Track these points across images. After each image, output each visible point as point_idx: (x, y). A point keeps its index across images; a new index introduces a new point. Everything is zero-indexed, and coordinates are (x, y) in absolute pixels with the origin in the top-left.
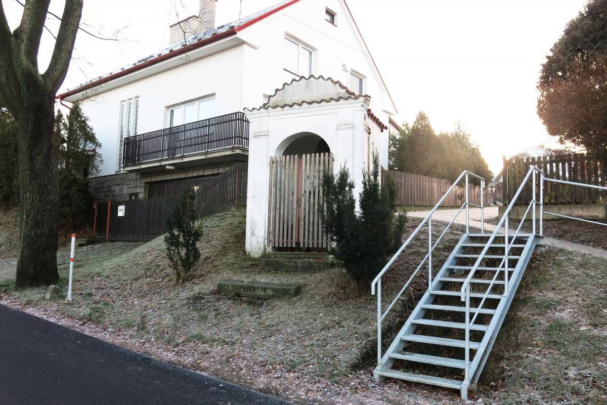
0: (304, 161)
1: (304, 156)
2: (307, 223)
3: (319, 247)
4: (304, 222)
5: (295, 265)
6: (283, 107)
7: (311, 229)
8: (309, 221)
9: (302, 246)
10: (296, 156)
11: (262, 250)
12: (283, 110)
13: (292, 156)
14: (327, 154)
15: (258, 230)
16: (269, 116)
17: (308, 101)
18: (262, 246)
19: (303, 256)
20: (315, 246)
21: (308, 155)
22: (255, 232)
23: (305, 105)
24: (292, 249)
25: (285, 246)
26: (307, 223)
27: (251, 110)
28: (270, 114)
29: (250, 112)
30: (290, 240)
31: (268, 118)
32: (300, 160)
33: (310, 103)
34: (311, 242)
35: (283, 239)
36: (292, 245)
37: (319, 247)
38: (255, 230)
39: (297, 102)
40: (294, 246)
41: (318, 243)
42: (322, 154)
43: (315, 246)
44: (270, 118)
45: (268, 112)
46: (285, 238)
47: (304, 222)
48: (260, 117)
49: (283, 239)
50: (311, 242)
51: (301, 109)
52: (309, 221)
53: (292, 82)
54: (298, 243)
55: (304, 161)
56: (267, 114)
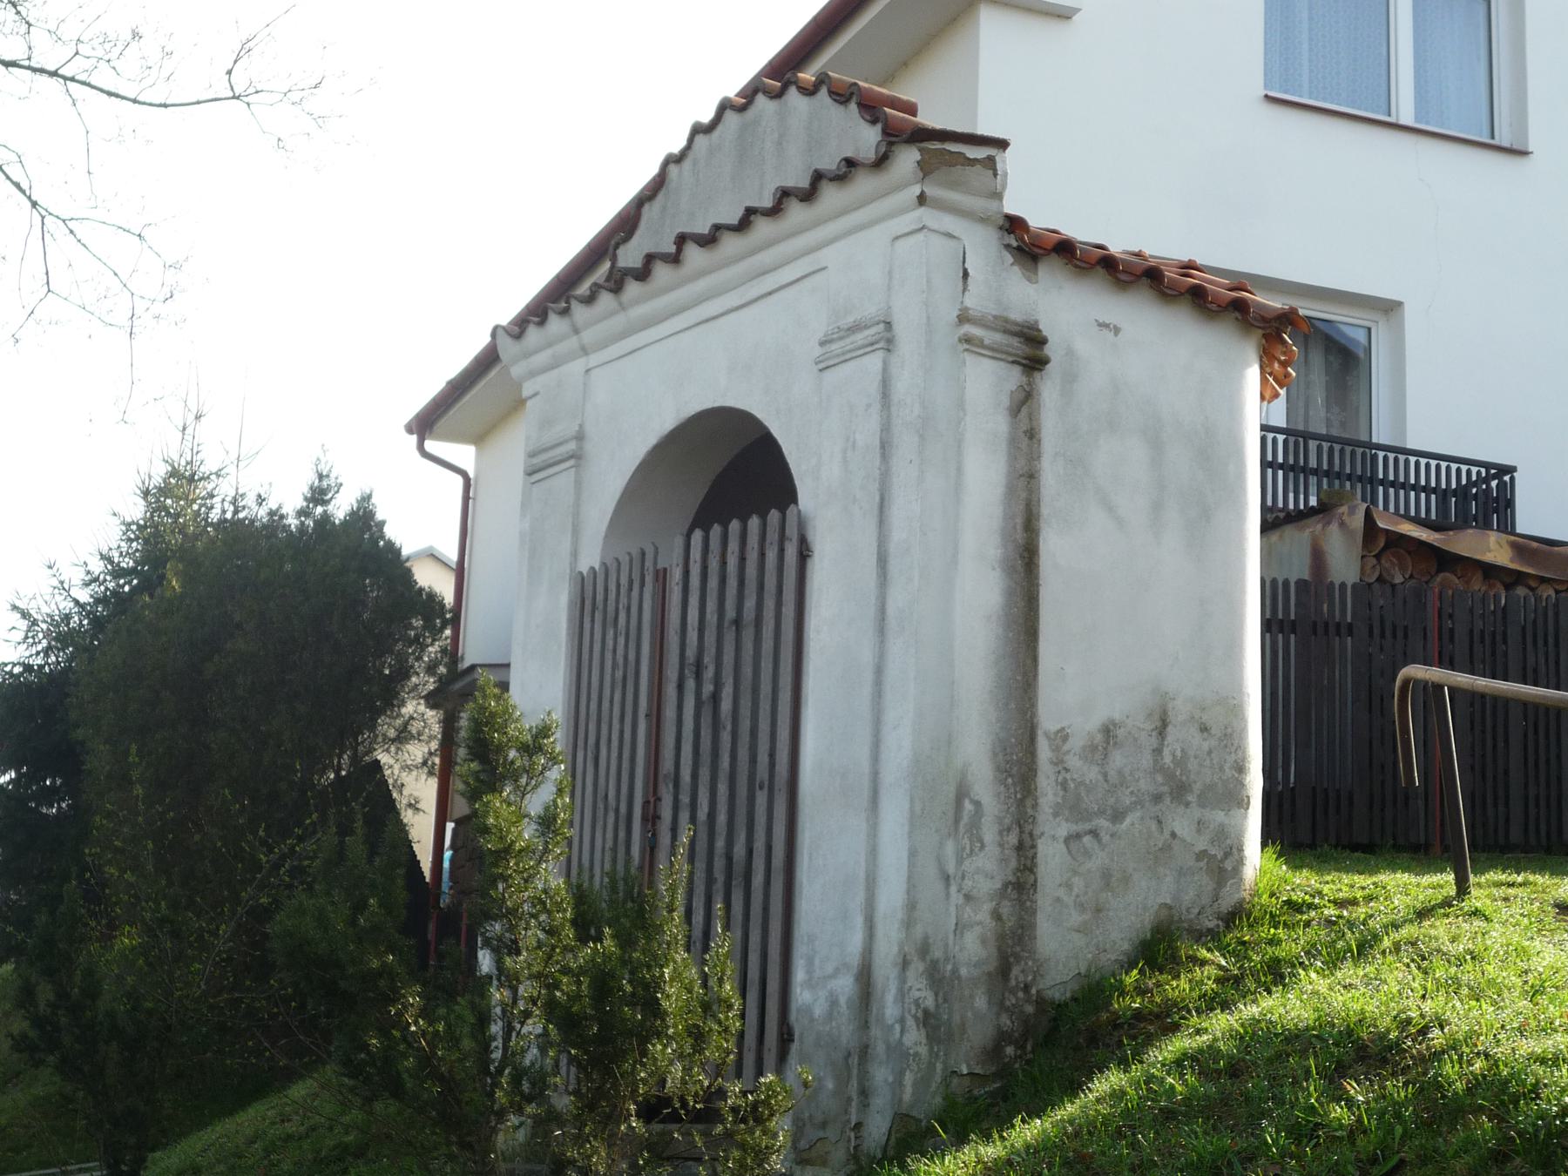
16: (585, 351)
28: (588, 336)
44: (594, 359)
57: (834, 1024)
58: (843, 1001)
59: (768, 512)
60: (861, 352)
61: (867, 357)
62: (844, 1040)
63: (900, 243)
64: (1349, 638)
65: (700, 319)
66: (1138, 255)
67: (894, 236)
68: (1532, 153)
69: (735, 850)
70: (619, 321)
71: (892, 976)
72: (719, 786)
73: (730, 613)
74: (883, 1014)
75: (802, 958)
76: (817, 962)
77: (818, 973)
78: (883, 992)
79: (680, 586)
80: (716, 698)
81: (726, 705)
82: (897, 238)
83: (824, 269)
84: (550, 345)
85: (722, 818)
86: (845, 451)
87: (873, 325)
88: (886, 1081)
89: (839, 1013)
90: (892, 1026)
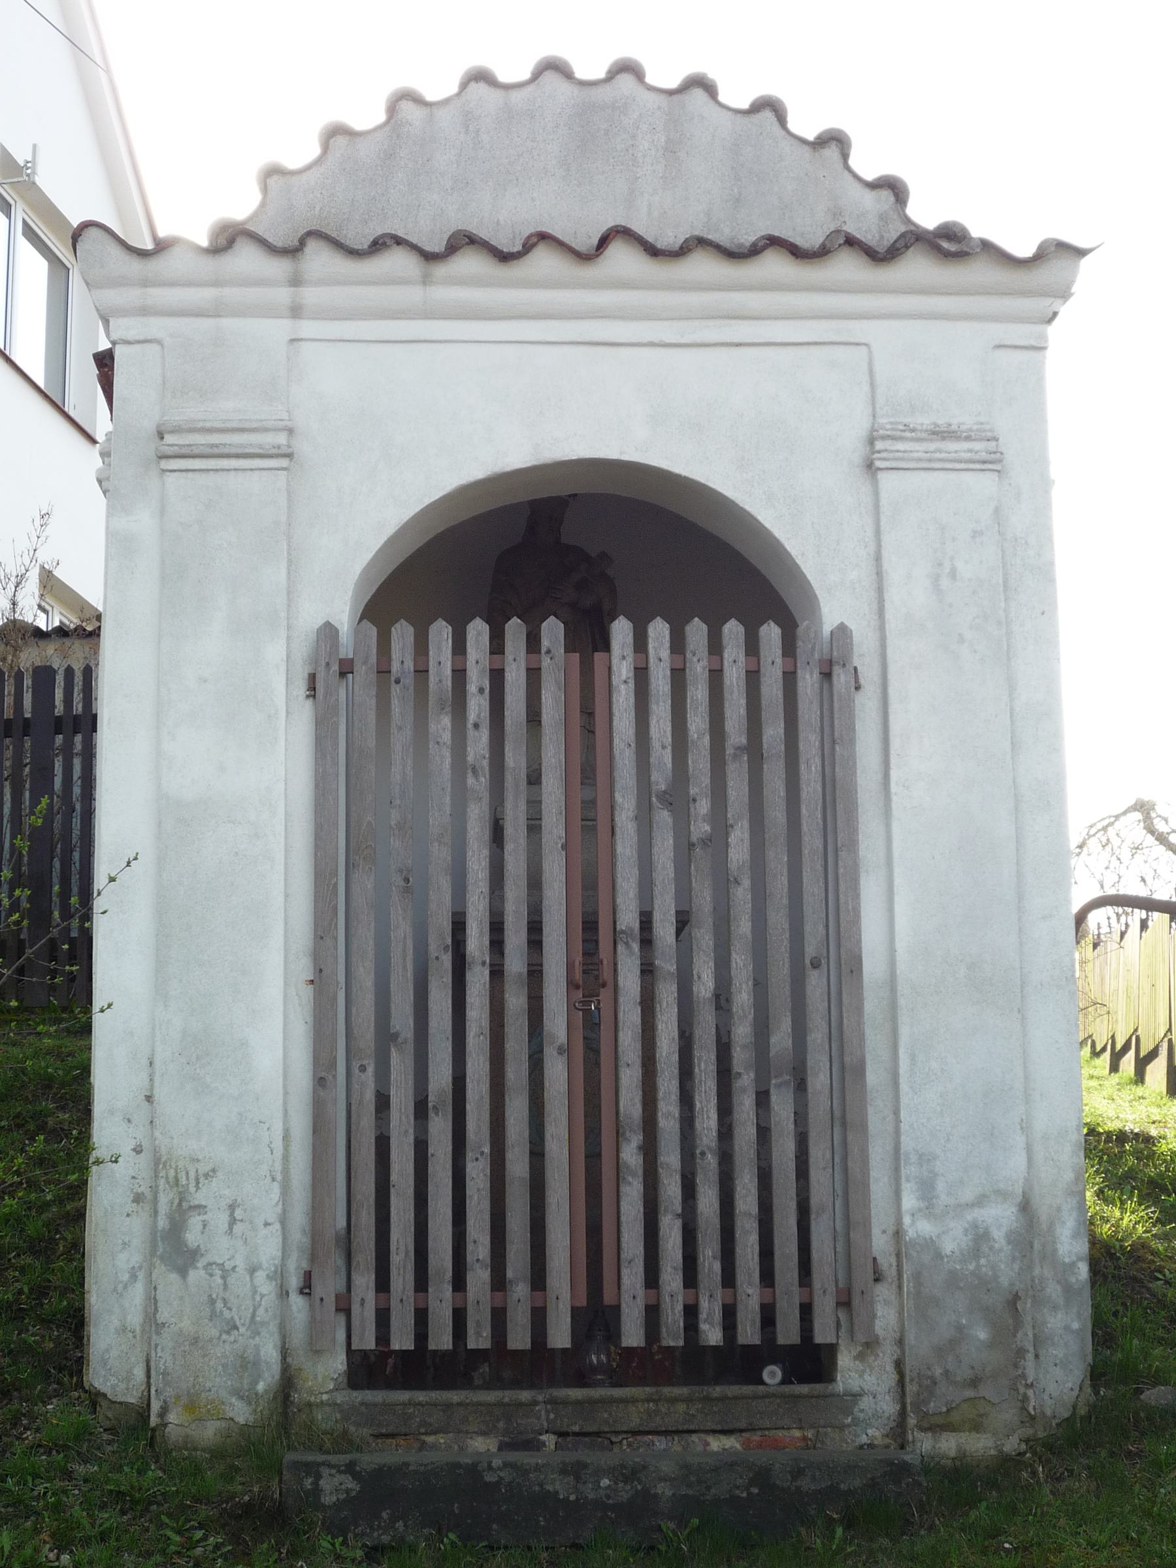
0: (623, 669)
2: (670, 1157)
3: (742, 1340)
4: (650, 1150)
5: (625, 1493)
7: (708, 1201)
10: (553, 630)
11: (267, 1382)
12: (426, 280)
13: (659, 631)
14: (771, 633)
15: (219, 1219)
16: (296, 312)
18: (269, 1351)
19: (634, 1417)
20: (479, 1338)
21: (659, 631)
22: (192, 1237)
25: (402, 1340)
26: (670, 1157)
27: (312, 246)
28: (311, 295)
29: (135, 266)
30: (520, 1291)
31: (280, 328)
32: (587, 670)
34: (710, 1309)
36: (421, 1335)
37: (742, 1340)
38: (195, 1221)
39: (483, 234)
40: (560, 1336)
42: (697, 631)
44: (308, 328)
45: (296, 281)
46: (479, 1278)
47: (650, 1150)
49: (459, 1283)
50: (710, 1309)
53: (537, 75)
55: (623, 669)
56: (283, 295)
60: (978, 466)
62: (1004, 1281)
63: (1003, 354)
64: (28, 715)
65: (588, 338)
67: (997, 343)
70: (414, 294)
71: (161, 1194)
72: (734, 955)
74: (1055, 1250)
75: (908, 1180)
76: (940, 1186)
77: (943, 1199)
78: (1051, 1225)
79: (632, 685)
82: (999, 347)
83: (35, 146)
84: (216, 283)
86: (936, 579)
87: (981, 440)
88: (1067, 1328)
89: (991, 1248)
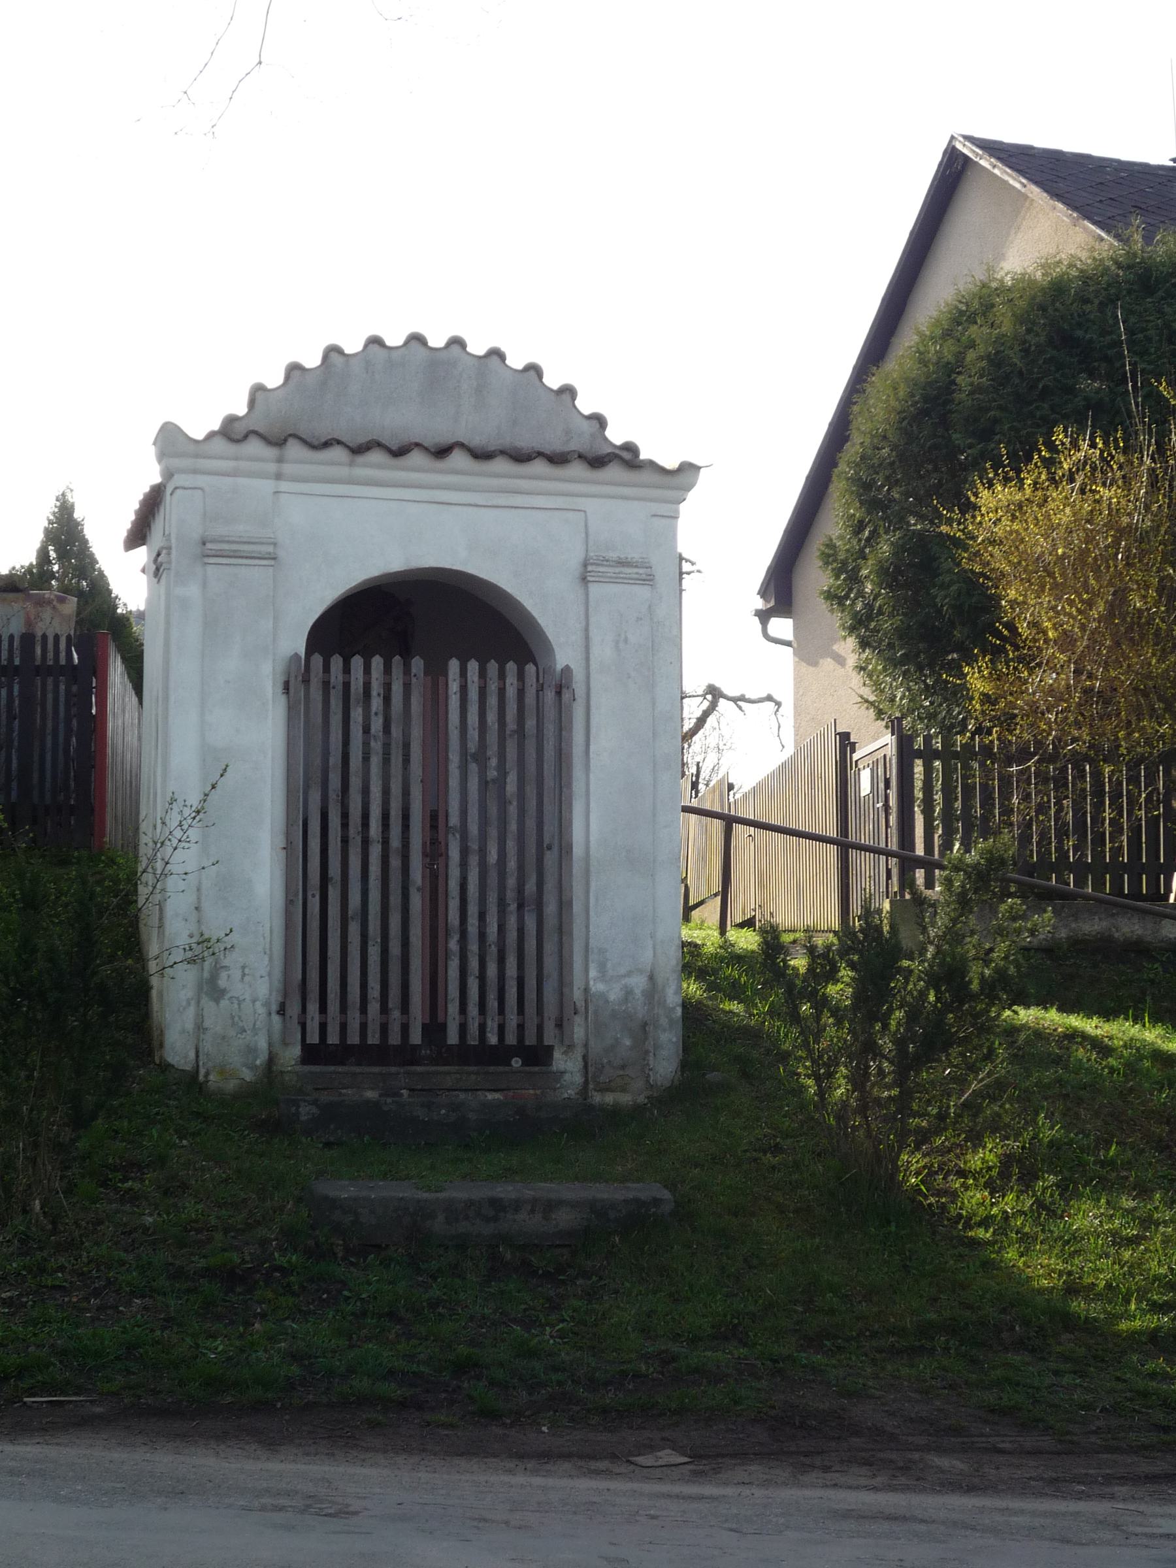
0: (454, 687)
1: (454, 665)
3: (330, 1042)
6: (358, 450)
7: (492, 970)
8: (482, 936)
9: (453, 1038)
12: (351, 464)
15: (236, 974)
16: (279, 477)
17: (476, 441)
18: (263, 1044)
20: (354, 1039)
23: (458, 459)
24: (406, 1055)
27: (291, 442)
28: (288, 468)
31: (268, 486)
32: (435, 684)
33: (481, 455)
35: (364, 1010)
37: (330, 1042)
38: (224, 974)
40: (416, 1037)
41: (344, 1027)
43: (373, 1039)
44: (284, 486)
45: (280, 460)
46: (374, 1008)
48: (234, 473)
49: (364, 1010)
50: (492, 1025)
51: (441, 472)
52: (482, 936)
54: (434, 1028)
55: (454, 687)
56: (272, 467)
57: (629, 1005)
58: (638, 992)
59: (488, 661)
61: (637, 586)
66: (154, 444)
68: (688, 471)
69: (527, 887)
70: (344, 471)
73: (511, 725)
80: (501, 781)
81: (511, 787)
84: (236, 459)
85: (512, 864)
90: (674, 1008)
